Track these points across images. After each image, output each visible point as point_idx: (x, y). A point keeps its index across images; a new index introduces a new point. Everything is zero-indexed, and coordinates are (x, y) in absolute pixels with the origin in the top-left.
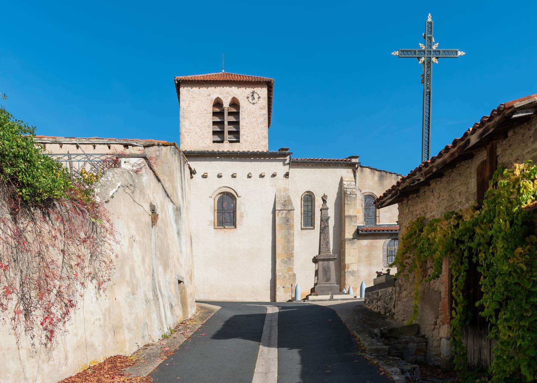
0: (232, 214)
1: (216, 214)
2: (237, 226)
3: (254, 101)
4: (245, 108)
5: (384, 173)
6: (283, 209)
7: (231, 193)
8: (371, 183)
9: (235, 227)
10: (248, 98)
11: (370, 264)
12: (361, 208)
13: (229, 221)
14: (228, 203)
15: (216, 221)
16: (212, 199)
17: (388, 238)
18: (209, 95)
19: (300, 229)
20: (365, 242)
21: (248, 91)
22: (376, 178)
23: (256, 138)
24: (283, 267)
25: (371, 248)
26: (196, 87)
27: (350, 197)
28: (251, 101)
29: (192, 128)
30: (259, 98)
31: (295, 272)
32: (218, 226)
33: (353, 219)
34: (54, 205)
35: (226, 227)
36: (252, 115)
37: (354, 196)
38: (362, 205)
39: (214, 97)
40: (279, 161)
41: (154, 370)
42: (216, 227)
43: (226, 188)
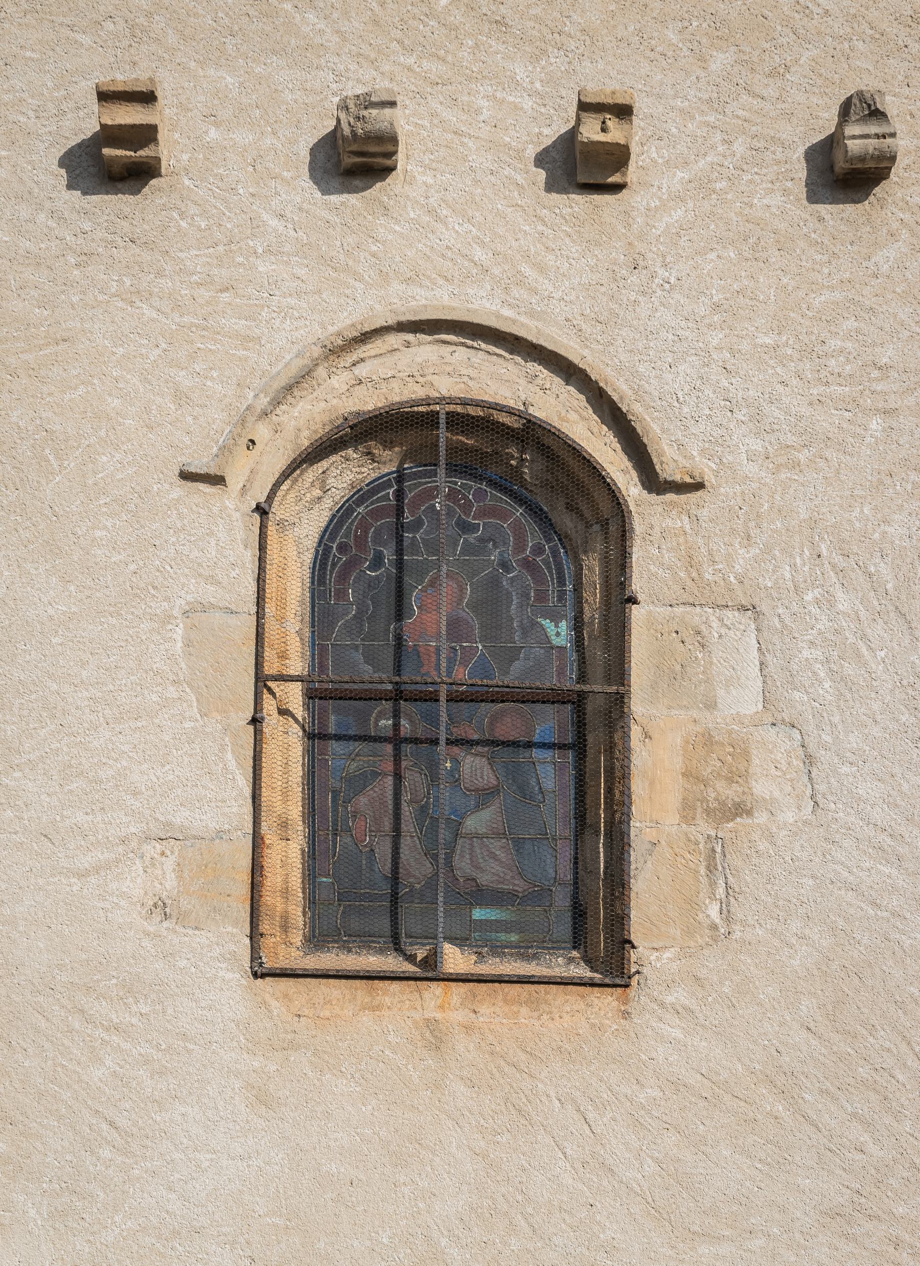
0: (550, 773)
1: (287, 747)
2: (654, 948)
7: (534, 435)
9: (611, 963)
13: (492, 865)
14: (490, 602)
15: (287, 857)
16: (231, 510)
31: (628, 180)
32: (316, 939)
34: (507, 454)
35: (455, 959)
41: (576, 809)
42: (288, 951)
43: (426, 351)
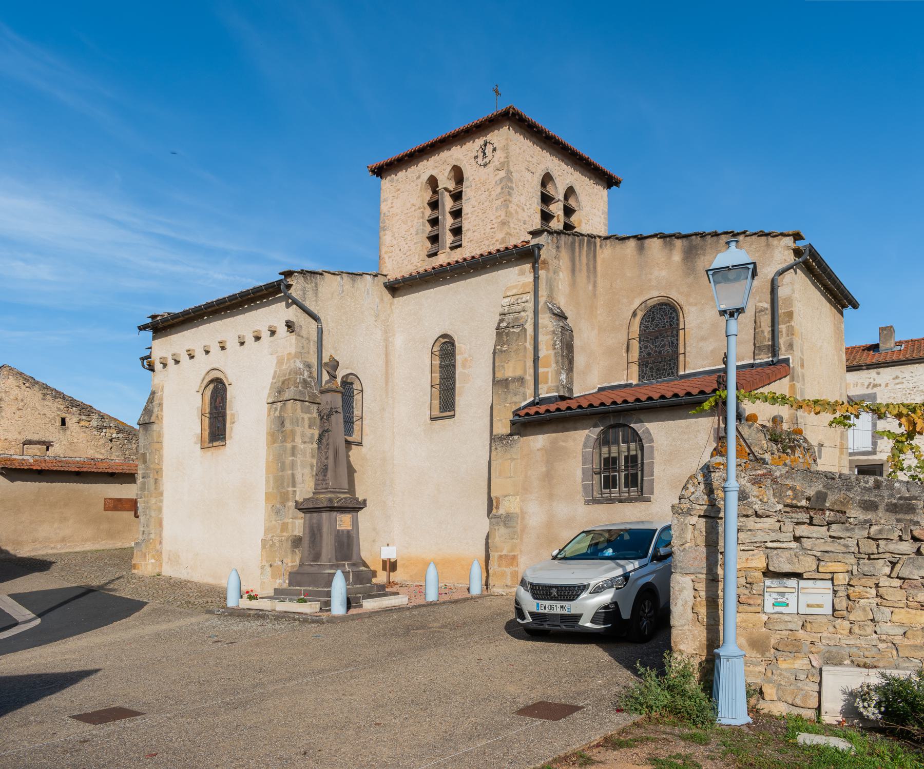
3: (487, 160)
4: (471, 179)
5: (696, 240)
6: (275, 399)
8: (664, 273)
10: (476, 157)
11: (551, 496)
12: (552, 352)
17: (595, 426)
18: (419, 177)
19: (429, 421)
20: (539, 441)
21: (474, 146)
22: (677, 257)
23: (488, 230)
24: (274, 522)
25: (553, 455)
26: (401, 170)
27: (507, 334)
28: (480, 160)
29: (395, 242)
30: (494, 150)
33: (512, 387)
36: (483, 189)
37: (517, 330)
38: (554, 344)
39: (425, 177)
40: (279, 300)
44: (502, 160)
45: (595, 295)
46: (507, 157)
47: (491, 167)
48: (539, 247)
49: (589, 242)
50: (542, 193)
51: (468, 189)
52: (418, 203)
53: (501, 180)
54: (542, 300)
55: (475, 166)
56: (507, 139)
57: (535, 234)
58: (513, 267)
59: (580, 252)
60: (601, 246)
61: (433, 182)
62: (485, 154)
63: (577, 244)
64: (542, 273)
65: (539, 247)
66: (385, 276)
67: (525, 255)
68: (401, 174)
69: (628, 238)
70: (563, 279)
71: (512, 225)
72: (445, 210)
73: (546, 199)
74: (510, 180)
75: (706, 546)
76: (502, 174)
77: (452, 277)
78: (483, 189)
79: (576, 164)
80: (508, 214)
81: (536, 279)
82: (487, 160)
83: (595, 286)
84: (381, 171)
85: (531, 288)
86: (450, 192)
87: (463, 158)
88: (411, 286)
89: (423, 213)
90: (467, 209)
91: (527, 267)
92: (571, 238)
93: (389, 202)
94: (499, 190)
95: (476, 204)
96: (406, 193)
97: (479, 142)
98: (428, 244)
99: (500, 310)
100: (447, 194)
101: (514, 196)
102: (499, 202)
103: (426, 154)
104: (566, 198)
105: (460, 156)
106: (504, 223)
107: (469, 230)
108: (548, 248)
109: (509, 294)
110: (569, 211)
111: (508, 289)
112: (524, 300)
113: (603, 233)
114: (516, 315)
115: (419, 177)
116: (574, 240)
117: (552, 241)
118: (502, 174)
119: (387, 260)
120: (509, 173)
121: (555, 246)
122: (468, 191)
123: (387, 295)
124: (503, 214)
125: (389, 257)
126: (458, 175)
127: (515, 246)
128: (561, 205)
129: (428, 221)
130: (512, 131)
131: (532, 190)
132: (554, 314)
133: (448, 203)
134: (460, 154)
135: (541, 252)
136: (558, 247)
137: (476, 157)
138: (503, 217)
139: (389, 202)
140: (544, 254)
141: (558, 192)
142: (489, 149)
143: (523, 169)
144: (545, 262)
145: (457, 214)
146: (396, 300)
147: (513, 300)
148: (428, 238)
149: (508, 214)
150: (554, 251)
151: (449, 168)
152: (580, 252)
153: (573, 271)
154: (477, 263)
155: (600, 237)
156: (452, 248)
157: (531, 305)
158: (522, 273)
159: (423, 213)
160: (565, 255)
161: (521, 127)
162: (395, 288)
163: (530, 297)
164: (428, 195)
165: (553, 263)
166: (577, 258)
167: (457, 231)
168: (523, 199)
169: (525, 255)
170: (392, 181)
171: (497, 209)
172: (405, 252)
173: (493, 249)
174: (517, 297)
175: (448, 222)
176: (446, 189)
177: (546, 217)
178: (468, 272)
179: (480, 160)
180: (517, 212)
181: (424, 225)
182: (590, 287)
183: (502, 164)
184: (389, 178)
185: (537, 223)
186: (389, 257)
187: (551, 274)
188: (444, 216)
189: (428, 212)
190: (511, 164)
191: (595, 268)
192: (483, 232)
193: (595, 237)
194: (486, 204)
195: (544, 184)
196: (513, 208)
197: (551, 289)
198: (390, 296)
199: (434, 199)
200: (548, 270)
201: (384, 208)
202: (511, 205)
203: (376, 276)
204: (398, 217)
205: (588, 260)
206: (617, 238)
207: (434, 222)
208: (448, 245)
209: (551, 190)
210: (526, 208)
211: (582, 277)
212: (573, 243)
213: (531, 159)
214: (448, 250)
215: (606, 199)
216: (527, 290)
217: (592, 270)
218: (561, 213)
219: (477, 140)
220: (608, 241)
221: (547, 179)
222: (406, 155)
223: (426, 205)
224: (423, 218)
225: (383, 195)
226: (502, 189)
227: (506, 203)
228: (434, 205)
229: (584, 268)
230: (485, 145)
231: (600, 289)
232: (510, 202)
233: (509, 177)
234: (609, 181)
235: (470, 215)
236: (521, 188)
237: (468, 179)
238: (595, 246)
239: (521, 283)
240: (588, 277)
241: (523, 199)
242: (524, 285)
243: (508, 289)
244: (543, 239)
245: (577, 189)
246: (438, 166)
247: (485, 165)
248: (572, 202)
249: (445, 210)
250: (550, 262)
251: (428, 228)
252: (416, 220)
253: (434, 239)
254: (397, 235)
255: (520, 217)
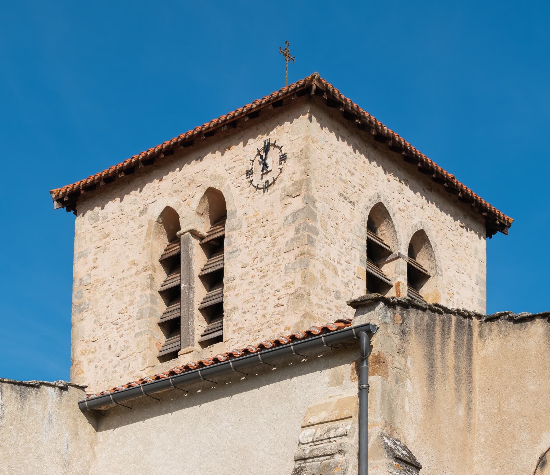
3: (269, 178)
4: (240, 213)
10: (249, 173)
18: (144, 212)
21: (244, 152)
23: (271, 309)
26: (112, 198)
28: (256, 178)
29: (99, 333)
30: (283, 158)
36: (261, 231)
39: (156, 211)
44: (297, 177)
45: (469, 426)
46: (306, 173)
47: (276, 191)
48: (369, 330)
49: (459, 325)
50: (369, 241)
51: (235, 234)
52: (143, 259)
53: (295, 215)
54: (374, 432)
55: (248, 190)
56: (306, 138)
57: (359, 305)
58: (320, 369)
59: (443, 343)
60: (481, 334)
61: (170, 220)
62: (265, 166)
63: (438, 329)
64: (374, 380)
65: (369, 330)
66: (83, 388)
67: (344, 345)
68: (113, 206)
69: (531, 318)
70: (412, 392)
71: (314, 300)
72: (193, 265)
73: (376, 253)
74: (312, 215)
75: (71, 304)
76: (297, 203)
77: (206, 389)
78: (261, 231)
79: (430, 189)
80: (307, 278)
81: (363, 391)
82: (269, 178)
83: (469, 408)
84: (75, 201)
85: (353, 409)
86: (201, 238)
87: (226, 175)
88: (130, 408)
89: (152, 278)
90: (232, 269)
91: (347, 369)
92: (426, 316)
93: (91, 257)
94: (291, 234)
95: (249, 260)
96: (121, 242)
97: (256, 144)
98: (161, 337)
99: (297, 451)
100: (195, 243)
101: (319, 245)
102: (291, 257)
103: (158, 167)
104: (412, 252)
105: (221, 171)
106: (299, 296)
107: (235, 308)
108: (386, 331)
109: (312, 420)
110: (416, 277)
111: (310, 411)
112: (341, 431)
113: (482, 310)
114: (326, 460)
115: (144, 212)
116: (433, 320)
117: (393, 320)
118: (297, 203)
119: (85, 366)
120: (310, 201)
121: (398, 329)
122: (234, 237)
123: (85, 426)
124: (298, 278)
125: (90, 361)
126: (216, 206)
127: (325, 330)
128: (402, 265)
129: (161, 293)
130: (315, 125)
131: (350, 236)
132: (397, 459)
133: (197, 260)
134: (221, 168)
135: (374, 341)
136: (403, 332)
137: (249, 173)
138: (298, 284)
139: (91, 257)
140: (378, 344)
141: (398, 240)
142: (273, 157)
143: (335, 195)
144: (379, 360)
145: (214, 279)
146: (102, 435)
147: (320, 431)
148: (160, 324)
149: (307, 278)
150: (396, 339)
151: (200, 194)
152: (443, 343)
153: (431, 378)
154: (254, 362)
155: (479, 316)
156: (205, 344)
157: (353, 441)
158: (337, 381)
159: (152, 278)
160: (415, 347)
161: (331, 117)
162: (102, 412)
163: (351, 426)
164: (160, 245)
165: (394, 362)
166: (438, 354)
167: (214, 312)
168: (334, 251)
169: (344, 345)
170: (95, 218)
171: (287, 269)
172: (114, 341)
173: (283, 334)
174: (328, 425)
175: (198, 294)
176: (194, 233)
177: (376, 284)
178: (236, 381)
179: (256, 178)
180: (323, 276)
181: (153, 301)
182: (462, 411)
183: (298, 185)
184: (89, 213)
185: (360, 290)
186: (90, 361)
187: (391, 383)
188: (190, 283)
189: (161, 276)
190: (313, 184)
191: (470, 374)
192: (261, 312)
193: (470, 317)
194: (267, 260)
195: (372, 226)
196: (316, 267)
197: (391, 410)
198: (90, 428)
199: (174, 250)
200: (385, 374)
201: (80, 268)
202: (313, 262)
203: (64, 388)
204: (106, 286)
205: (457, 360)
206: (511, 319)
207: (172, 295)
208: (197, 338)
209: (384, 236)
210: (339, 268)
211: (446, 389)
212: (431, 326)
213: (349, 178)
214: (197, 347)
215: (483, 256)
216: (346, 413)
217: (465, 377)
218: (403, 279)
219: (251, 141)
220: (494, 324)
221: (378, 216)
222: (121, 170)
223: (158, 264)
224: (151, 287)
225: (79, 246)
226: (297, 231)
227: (304, 259)
228: (172, 263)
229: (451, 374)
230: (266, 150)
231: (478, 416)
232: (312, 256)
233: (309, 210)
234: (489, 224)
235: (237, 282)
236: (331, 230)
237: (234, 213)
238: (471, 334)
239: (334, 400)
240: (458, 391)
241: (334, 251)
242: (341, 404)
243: (310, 411)
244: (376, 316)
245: (432, 235)
246: (179, 189)
247: (266, 187)
248: (423, 261)
249: (193, 265)
250: (389, 359)
251: (161, 306)
252: (138, 293)
253: (172, 327)
254: (103, 320)
255: (328, 285)
